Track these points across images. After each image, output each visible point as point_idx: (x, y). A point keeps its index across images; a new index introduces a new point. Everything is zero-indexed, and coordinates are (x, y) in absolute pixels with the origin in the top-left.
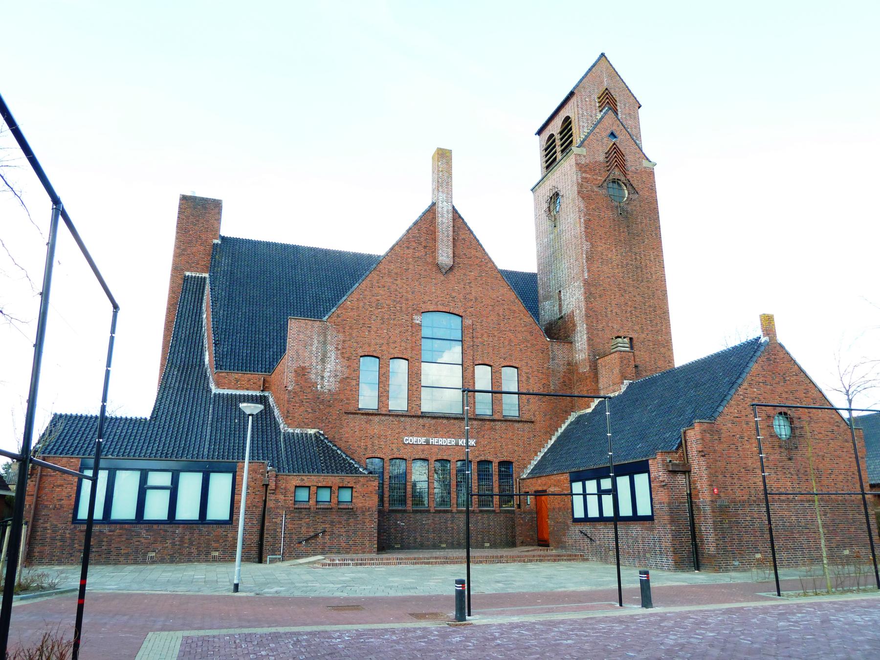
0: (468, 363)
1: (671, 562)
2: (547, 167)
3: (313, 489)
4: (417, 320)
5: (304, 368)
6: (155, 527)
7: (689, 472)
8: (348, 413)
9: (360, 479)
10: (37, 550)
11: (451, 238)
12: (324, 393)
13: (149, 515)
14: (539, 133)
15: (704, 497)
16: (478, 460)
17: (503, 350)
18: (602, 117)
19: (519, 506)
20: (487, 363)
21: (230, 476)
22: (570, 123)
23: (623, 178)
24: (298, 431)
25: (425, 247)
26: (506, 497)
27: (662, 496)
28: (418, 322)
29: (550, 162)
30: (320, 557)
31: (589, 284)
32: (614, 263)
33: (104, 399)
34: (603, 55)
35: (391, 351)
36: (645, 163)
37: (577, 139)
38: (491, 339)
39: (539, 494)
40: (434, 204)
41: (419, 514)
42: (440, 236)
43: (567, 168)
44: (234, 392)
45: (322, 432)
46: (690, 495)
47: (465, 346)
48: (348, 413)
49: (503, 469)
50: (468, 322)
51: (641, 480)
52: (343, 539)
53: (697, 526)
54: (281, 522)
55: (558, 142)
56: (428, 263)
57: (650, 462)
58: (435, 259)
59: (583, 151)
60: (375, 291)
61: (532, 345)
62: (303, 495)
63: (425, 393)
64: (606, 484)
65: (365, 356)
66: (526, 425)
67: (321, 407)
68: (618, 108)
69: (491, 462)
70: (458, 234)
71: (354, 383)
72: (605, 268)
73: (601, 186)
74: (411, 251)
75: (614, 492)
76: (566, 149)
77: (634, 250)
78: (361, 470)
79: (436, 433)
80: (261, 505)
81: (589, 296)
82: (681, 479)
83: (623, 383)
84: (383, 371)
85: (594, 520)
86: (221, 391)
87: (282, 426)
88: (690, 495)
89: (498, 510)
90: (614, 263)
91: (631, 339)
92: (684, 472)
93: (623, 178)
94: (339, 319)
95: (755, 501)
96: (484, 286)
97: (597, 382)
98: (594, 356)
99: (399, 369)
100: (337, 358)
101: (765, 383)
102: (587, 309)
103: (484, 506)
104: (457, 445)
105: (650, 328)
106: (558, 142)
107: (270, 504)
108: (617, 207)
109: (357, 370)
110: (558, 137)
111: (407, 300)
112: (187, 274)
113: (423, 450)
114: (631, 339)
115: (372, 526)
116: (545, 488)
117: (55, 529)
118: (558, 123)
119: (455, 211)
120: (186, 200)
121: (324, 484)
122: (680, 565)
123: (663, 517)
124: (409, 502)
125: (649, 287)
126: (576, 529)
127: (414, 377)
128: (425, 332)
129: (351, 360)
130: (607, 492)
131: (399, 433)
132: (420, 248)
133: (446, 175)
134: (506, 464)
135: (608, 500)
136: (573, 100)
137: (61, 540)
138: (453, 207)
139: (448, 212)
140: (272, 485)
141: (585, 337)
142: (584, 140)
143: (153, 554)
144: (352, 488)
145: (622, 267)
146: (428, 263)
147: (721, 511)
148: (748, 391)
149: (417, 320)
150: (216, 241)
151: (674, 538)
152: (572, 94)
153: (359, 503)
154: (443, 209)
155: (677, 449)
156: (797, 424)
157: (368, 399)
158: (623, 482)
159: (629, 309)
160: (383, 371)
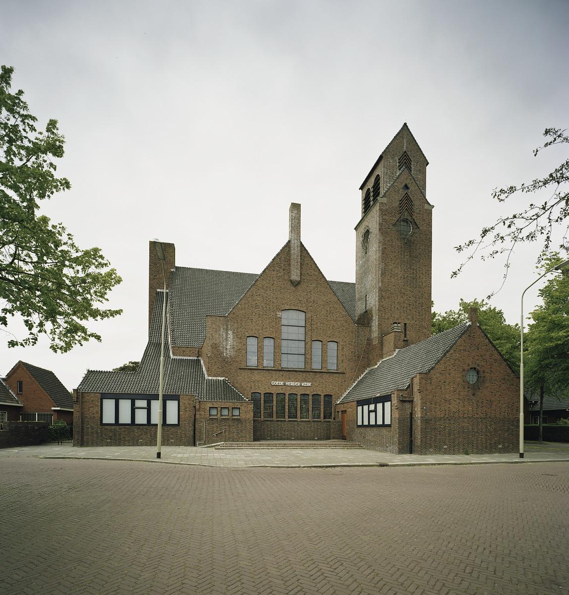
0: (308, 340)
1: (397, 448)
2: (365, 212)
3: (219, 409)
4: (279, 314)
5: (215, 344)
6: (141, 427)
7: (412, 401)
8: (241, 369)
9: (244, 404)
10: (85, 437)
11: (299, 264)
12: (228, 358)
13: (137, 421)
14: (361, 188)
15: (418, 414)
16: (313, 394)
17: (329, 332)
18: (400, 174)
19: (334, 419)
20: (319, 339)
21: (177, 402)
22: (379, 179)
23: (409, 218)
24: (215, 378)
25: (284, 270)
26: (327, 415)
27: (396, 415)
28: (279, 316)
29: (367, 206)
30: (223, 443)
31: (382, 290)
32: (399, 276)
33: (522, 313)
34: (405, 124)
35: (264, 333)
36: (426, 206)
37: (382, 191)
38: (322, 325)
39: (344, 412)
40: (289, 241)
41: (280, 422)
42: (292, 262)
43: (375, 211)
44: (182, 358)
45: (227, 379)
46: (411, 414)
47: (306, 330)
48: (241, 369)
49: (326, 399)
50: (309, 315)
51: (388, 405)
52: (235, 434)
53: (413, 430)
54: (202, 426)
55: (372, 194)
56: (285, 280)
57: (392, 395)
58: (290, 277)
59: (385, 200)
60: (255, 297)
61: (347, 329)
62: (214, 412)
63: (284, 357)
64: (372, 407)
65: (249, 336)
66: (340, 375)
67: (226, 365)
68: (412, 166)
69: (320, 395)
70: (304, 261)
71: (244, 352)
72: (393, 280)
73: (394, 225)
74: (275, 272)
75: (375, 411)
76: (375, 199)
77: (412, 267)
78: (245, 398)
79: (290, 379)
80: (193, 416)
81: (381, 298)
82: (407, 405)
83: (395, 351)
84: (260, 345)
85: (366, 426)
86: (176, 357)
87: (206, 376)
88: (411, 414)
89: (299, 420)
90: (399, 276)
91: (405, 324)
92: (409, 401)
93: (409, 218)
94: (234, 315)
95: (447, 418)
96: (319, 293)
97: (382, 350)
98: (382, 335)
99: (268, 344)
100: (234, 338)
101: (465, 350)
102: (379, 305)
103: (291, 418)
104: (301, 386)
105: (418, 317)
106: (372, 194)
107: (197, 416)
108: (404, 239)
109: (246, 344)
110: (372, 190)
111: (273, 303)
112: (158, 290)
113: (282, 389)
114: (405, 324)
115: (250, 426)
116: (346, 409)
117: (92, 428)
118: (372, 179)
119: (302, 245)
120: (153, 245)
121: (225, 406)
122: (401, 451)
123: (396, 426)
124: (275, 416)
125: (420, 291)
126: (358, 431)
127: (277, 348)
128: (284, 322)
129: (242, 338)
130: (372, 411)
131: (269, 379)
132: (281, 270)
133: (297, 221)
134: (328, 397)
135: (372, 415)
136: (382, 163)
137: (96, 433)
138: (301, 243)
139: (297, 247)
140: (197, 407)
141: (377, 323)
142: (387, 192)
143: (142, 441)
144: (239, 408)
145: (404, 278)
146: (285, 280)
147: (426, 421)
148: (453, 355)
149: (279, 314)
150: (172, 270)
151: (400, 436)
152: (381, 158)
153: (243, 416)
154: (295, 244)
155: (407, 388)
156: (481, 374)
157: (252, 361)
158: (380, 406)
159: (406, 306)
160: (260, 345)
